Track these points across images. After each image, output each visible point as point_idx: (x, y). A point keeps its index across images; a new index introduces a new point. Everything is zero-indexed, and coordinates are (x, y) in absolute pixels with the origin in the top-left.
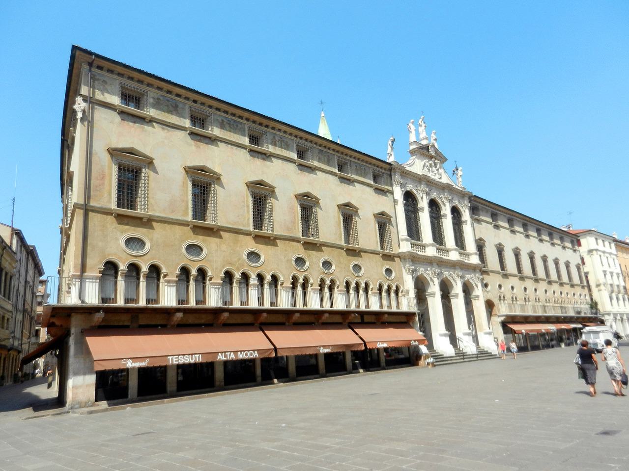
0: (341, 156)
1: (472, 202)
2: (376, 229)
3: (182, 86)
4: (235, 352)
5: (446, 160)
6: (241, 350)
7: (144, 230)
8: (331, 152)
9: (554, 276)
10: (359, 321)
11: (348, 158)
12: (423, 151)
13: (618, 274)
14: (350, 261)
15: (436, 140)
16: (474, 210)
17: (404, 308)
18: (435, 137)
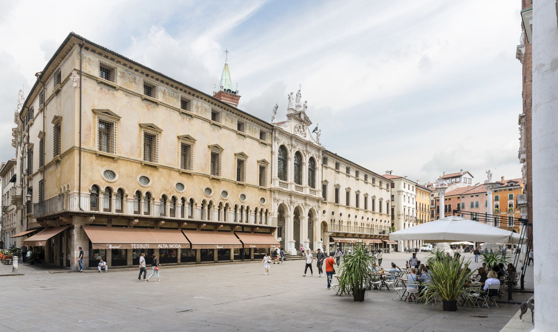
13: (413, 208)
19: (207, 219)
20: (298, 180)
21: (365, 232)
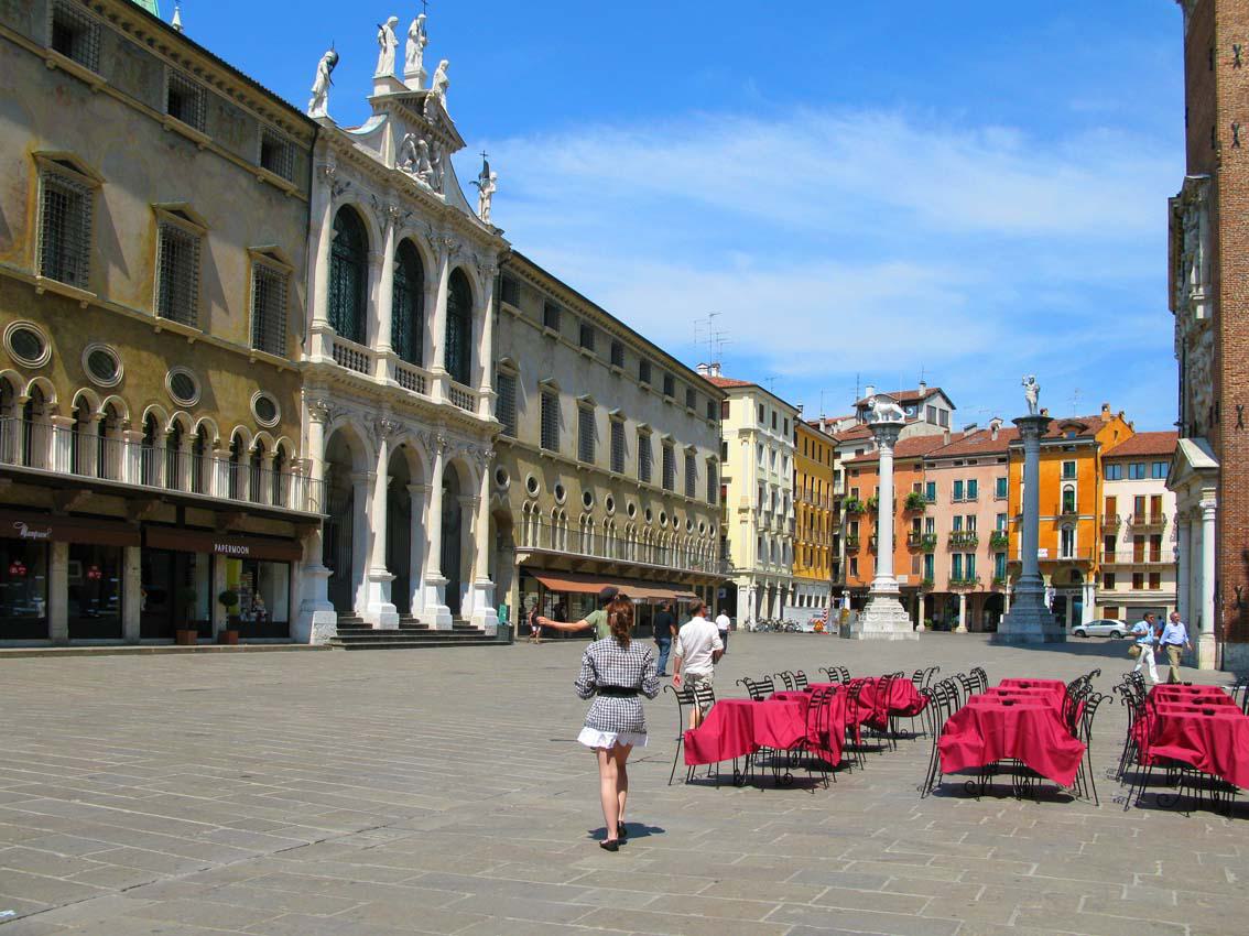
13: (786, 491)
15: (444, 85)
19: (19, 456)
20: (409, 342)
21: (633, 557)
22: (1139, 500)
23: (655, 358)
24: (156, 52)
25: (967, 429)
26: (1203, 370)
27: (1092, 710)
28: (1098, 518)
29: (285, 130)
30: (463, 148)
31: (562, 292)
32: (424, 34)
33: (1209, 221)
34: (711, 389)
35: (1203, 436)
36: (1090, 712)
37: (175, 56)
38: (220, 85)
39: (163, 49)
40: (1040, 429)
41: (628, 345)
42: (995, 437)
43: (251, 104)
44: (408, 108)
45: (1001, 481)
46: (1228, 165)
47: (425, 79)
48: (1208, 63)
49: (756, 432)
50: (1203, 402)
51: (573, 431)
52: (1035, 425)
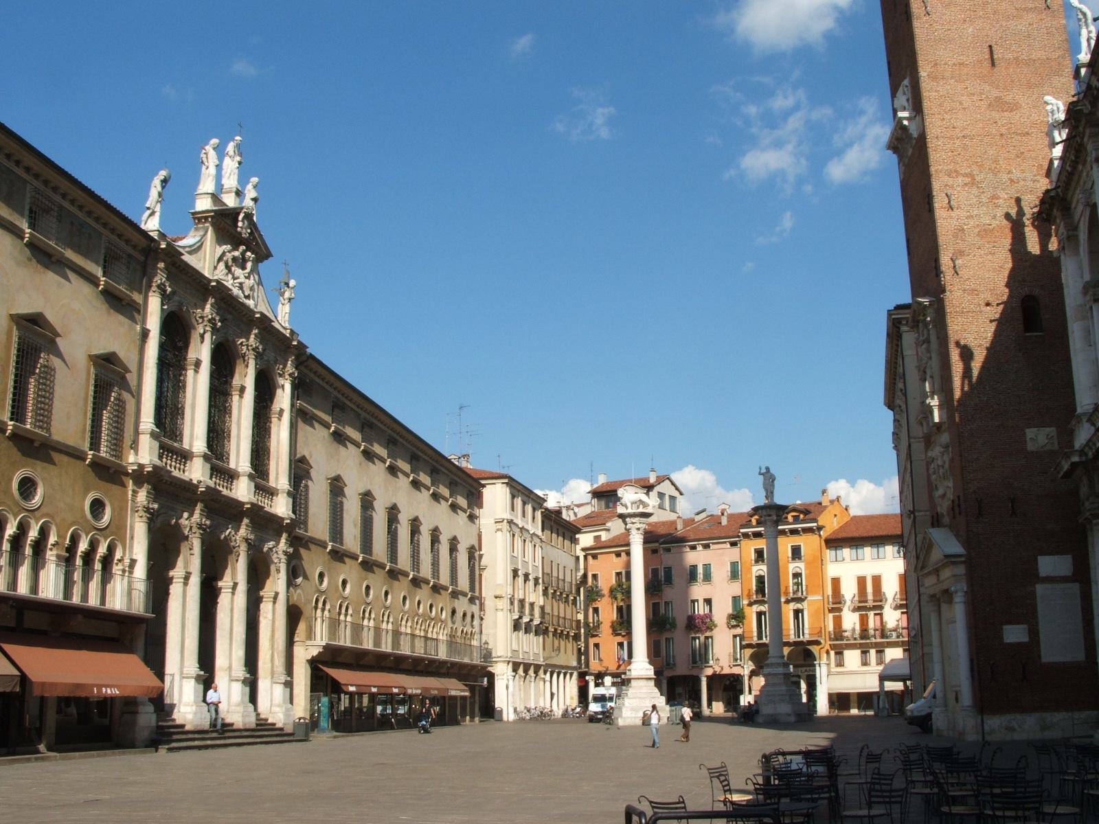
0: (42, 187)
1: (302, 368)
2: (87, 394)
3: (93, 192)
4: (100, 687)
5: (268, 255)
6: (106, 683)
7: (40, 465)
8: (20, 172)
9: (351, 539)
10: (13, 624)
11: (58, 199)
12: (224, 222)
14: (15, 467)
15: (255, 200)
16: (300, 388)
17: (117, 602)
18: (253, 194)
22: (861, 581)
23: (423, 452)
24: (20, 172)
25: (698, 514)
26: (943, 466)
27: (875, 776)
28: (826, 597)
29: (116, 238)
30: (271, 258)
31: (347, 391)
32: (240, 155)
33: (938, 338)
34: (470, 481)
35: (945, 526)
36: (876, 774)
37: (37, 176)
38: (72, 202)
39: (28, 170)
40: (777, 516)
41: (401, 440)
42: (724, 521)
43: (97, 219)
44: (224, 222)
45: (734, 565)
46: (951, 292)
47: (239, 194)
48: (927, 206)
49: (510, 522)
50: (943, 496)
51: (355, 525)
52: (773, 512)
